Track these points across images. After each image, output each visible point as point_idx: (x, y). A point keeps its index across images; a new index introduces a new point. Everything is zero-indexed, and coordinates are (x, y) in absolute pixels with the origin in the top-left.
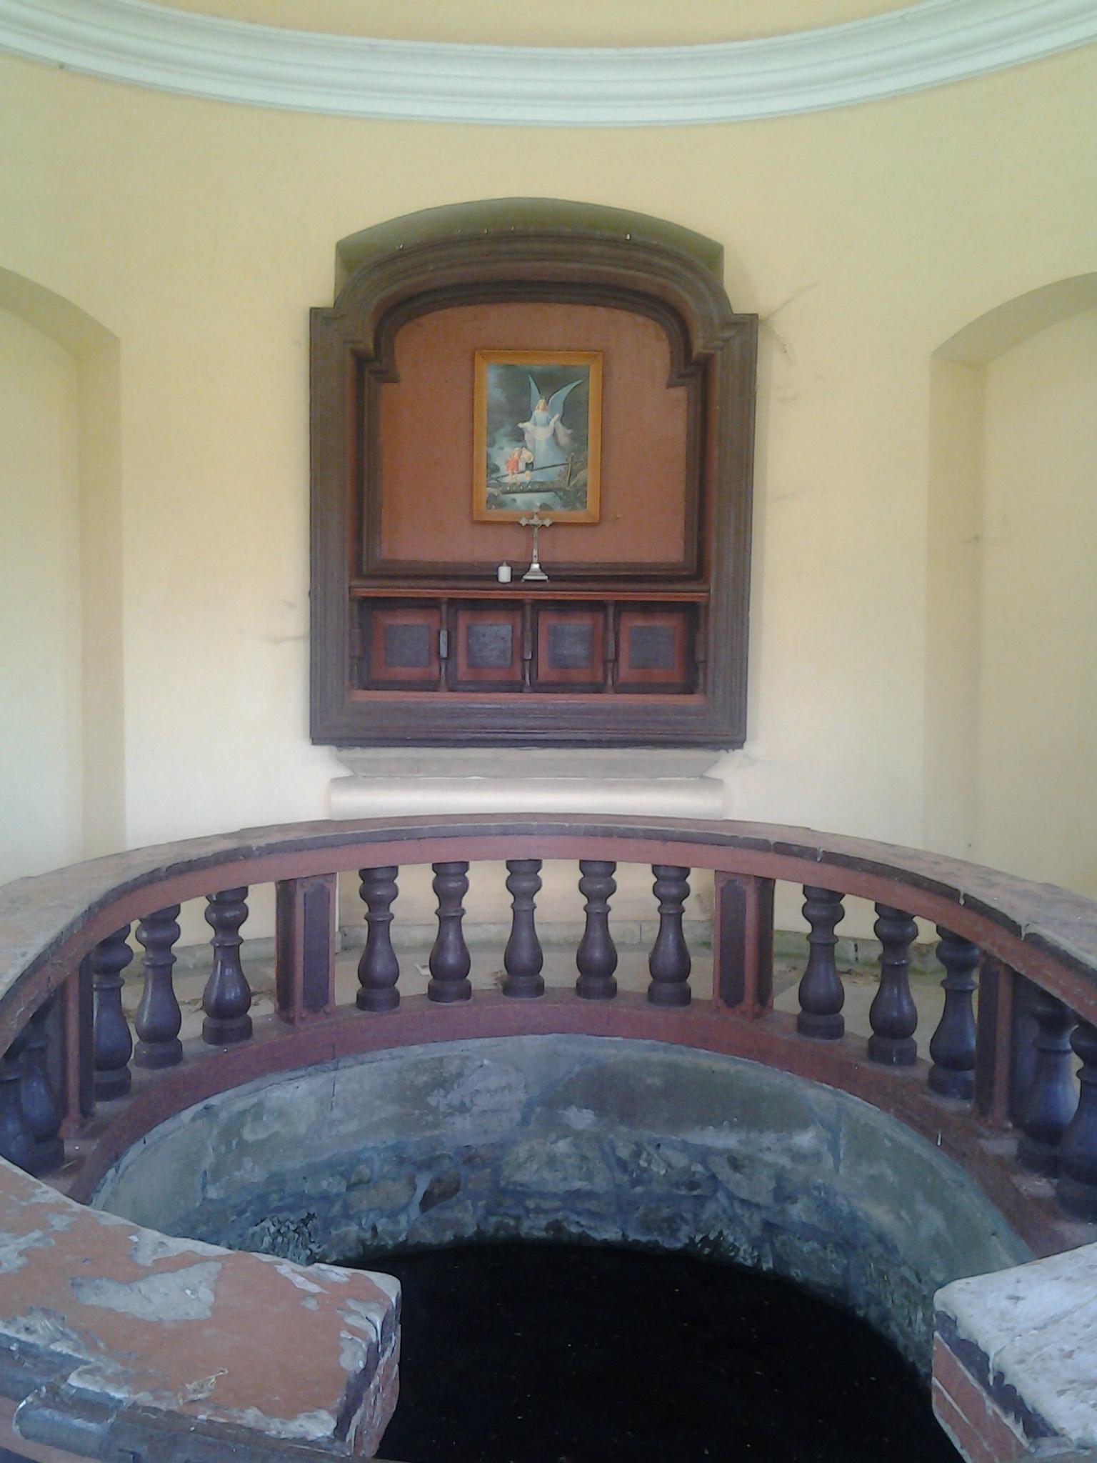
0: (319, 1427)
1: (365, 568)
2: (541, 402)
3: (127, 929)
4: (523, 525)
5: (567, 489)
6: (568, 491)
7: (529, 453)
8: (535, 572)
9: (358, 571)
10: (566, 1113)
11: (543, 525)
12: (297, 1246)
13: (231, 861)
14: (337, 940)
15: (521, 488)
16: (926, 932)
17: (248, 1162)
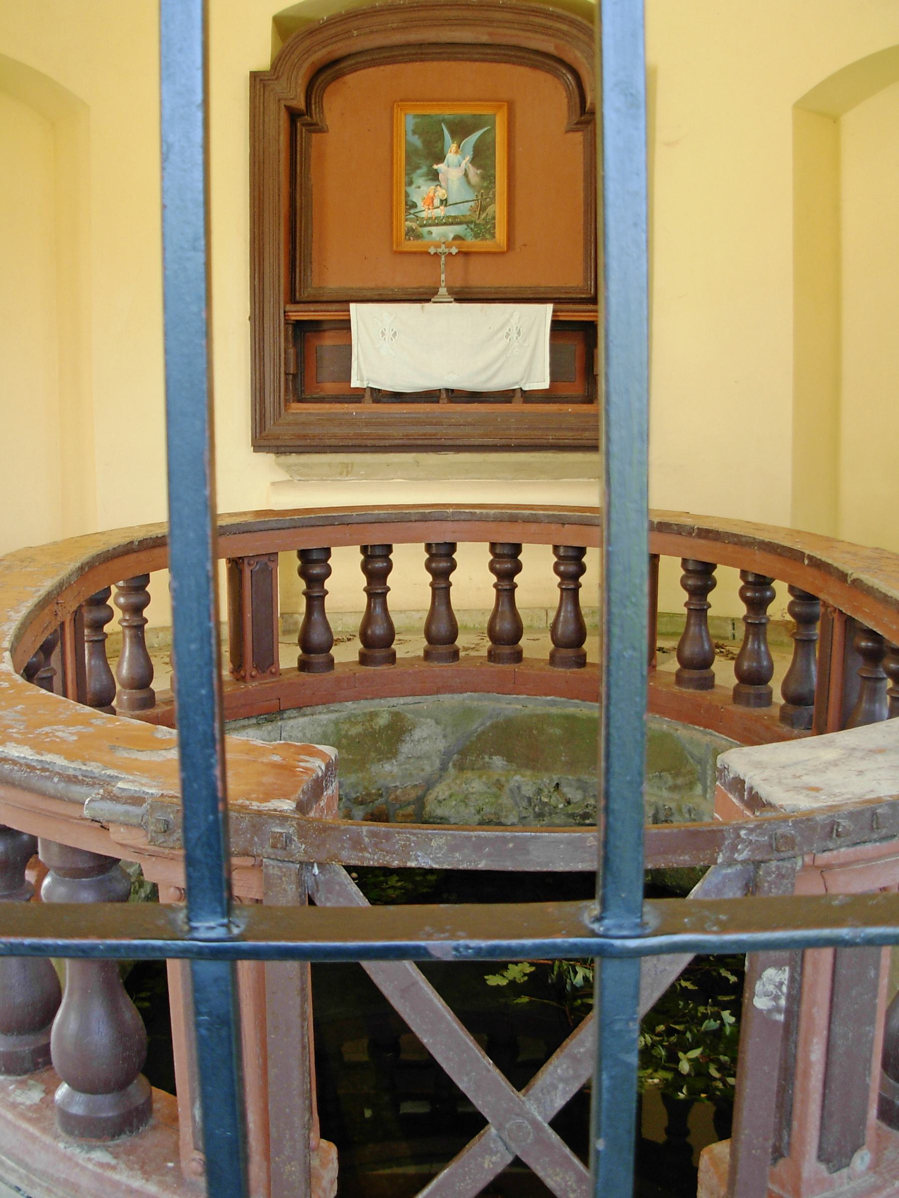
1: (297, 294)
2: (454, 147)
3: (108, 591)
4: (432, 253)
6: (479, 224)
7: (444, 191)
9: (292, 298)
14: (280, 625)
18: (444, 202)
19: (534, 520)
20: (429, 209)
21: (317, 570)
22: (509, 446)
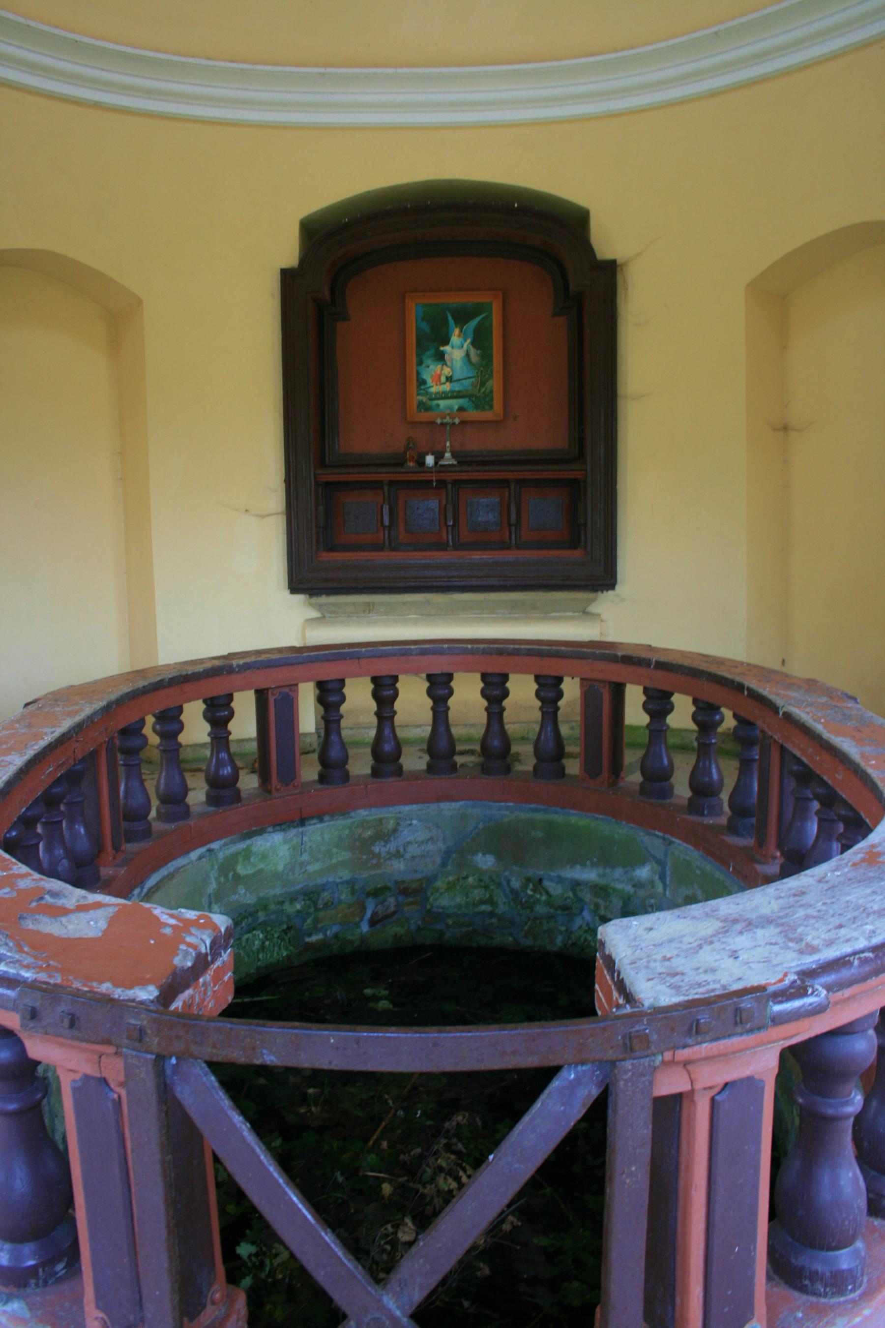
0: (147, 993)
1: (327, 459)
2: (457, 331)
3: (142, 722)
5: (478, 395)
8: (448, 460)
9: (321, 463)
10: (474, 858)
11: (454, 424)
12: (280, 948)
13: (218, 675)
15: (443, 395)
16: (729, 721)
17: (241, 890)
18: (450, 379)
19: (516, 653)
20: (437, 385)
21: (333, 699)
22: (506, 586)
